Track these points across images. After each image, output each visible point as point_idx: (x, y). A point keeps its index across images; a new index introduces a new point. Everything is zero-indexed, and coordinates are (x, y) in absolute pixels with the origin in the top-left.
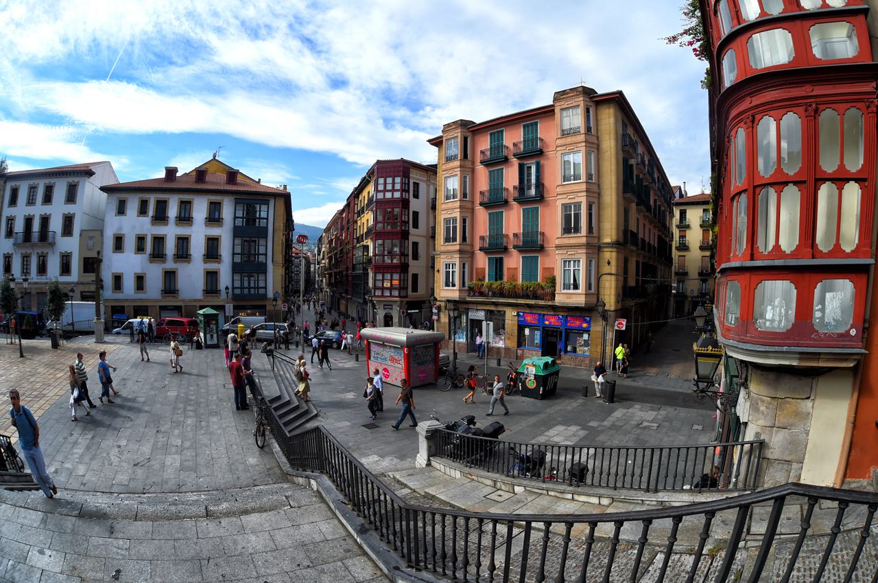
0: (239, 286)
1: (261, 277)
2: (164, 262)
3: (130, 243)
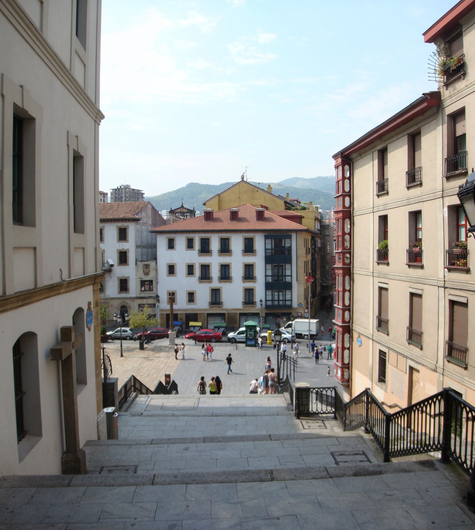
0: (271, 299)
1: (288, 293)
2: (211, 282)
3: (181, 270)
